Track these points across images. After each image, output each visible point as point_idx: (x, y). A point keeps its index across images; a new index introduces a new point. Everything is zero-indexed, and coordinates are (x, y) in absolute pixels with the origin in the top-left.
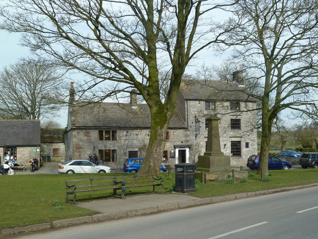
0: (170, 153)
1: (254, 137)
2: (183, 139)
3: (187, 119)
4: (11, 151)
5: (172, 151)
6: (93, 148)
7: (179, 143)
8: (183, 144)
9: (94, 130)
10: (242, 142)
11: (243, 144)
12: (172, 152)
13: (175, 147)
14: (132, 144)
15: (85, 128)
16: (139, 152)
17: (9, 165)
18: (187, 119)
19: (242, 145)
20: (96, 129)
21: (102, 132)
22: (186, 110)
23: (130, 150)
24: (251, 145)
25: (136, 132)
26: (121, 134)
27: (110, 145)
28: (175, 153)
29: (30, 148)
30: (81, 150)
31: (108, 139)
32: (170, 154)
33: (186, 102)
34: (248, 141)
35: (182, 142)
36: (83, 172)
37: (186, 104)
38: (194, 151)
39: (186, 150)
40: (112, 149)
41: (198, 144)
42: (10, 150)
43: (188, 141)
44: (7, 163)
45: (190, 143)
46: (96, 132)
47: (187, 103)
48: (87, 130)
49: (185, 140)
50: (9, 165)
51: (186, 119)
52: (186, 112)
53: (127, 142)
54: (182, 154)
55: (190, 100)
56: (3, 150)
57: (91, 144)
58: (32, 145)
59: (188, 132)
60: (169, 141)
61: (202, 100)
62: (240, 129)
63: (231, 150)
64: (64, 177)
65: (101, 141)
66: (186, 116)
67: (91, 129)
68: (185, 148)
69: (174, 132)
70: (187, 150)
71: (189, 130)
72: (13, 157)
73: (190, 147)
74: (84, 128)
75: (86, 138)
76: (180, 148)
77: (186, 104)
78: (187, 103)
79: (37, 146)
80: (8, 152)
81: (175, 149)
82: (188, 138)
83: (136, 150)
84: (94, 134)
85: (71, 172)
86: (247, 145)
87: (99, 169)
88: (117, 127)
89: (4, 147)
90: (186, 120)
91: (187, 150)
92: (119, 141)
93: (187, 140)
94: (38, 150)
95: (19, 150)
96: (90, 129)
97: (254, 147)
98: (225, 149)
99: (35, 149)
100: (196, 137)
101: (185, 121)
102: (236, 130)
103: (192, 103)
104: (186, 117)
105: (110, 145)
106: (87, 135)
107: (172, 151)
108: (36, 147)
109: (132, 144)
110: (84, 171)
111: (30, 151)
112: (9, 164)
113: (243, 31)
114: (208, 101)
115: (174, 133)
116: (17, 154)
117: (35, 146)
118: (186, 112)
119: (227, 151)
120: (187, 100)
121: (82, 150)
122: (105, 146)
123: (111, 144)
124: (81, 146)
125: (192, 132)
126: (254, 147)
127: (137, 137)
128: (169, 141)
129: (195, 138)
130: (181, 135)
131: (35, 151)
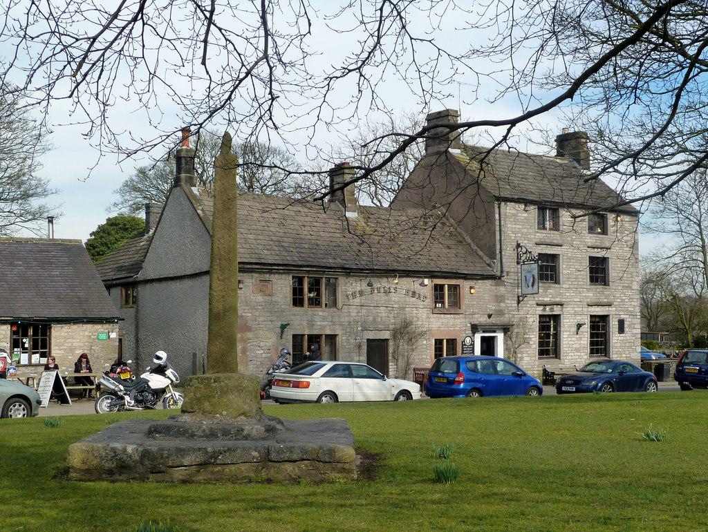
0: (463, 345)
1: (634, 306)
2: (492, 307)
3: (501, 252)
4: (33, 335)
5: (468, 340)
6: (279, 330)
7: (483, 319)
8: (493, 320)
9: (282, 273)
10: (611, 317)
11: (614, 324)
12: (468, 342)
13: (475, 328)
14: (374, 320)
15: (257, 267)
16: (391, 343)
17: (168, 378)
18: (501, 252)
19: (611, 327)
20: (287, 272)
21: (300, 281)
22: (498, 228)
23: (372, 335)
24: (629, 326)
25: (384, 283)
26: (348, 287)
27: (317, 320)
28: (473, 345)
29: (89, 326)
30: (249, 335)
31: (315, 302)
32: (463, 348)
33: (496, 206)
34: (623, 317)
35: (490, 316)
36: (360, 398)
37: (497, 210)
38: (514, 339)
39: (493, 337)
40: (328, 332)
41: (523, 320)
42: (31, 332)
43: (500, 313)
44: (160, 370)
45: (505, 319)
46: (287, 282)
47: (499, 207)
48: (264, 273)
49: (495, 310)
50: (168, 378)
51: (498, 252)
52: (498, 233)
53: (364, 311)
54: (488, 345)
55: (507, 200)
56: (9, 332)
57: (274, 319)
58: (97, 319)
59: (502, 289)
60: (460, 311)
61: (532, 202)
62: (557, 281)
63: (589, 339)
64: (485, 410)
65: (298, 309)
66: (498, 243)
67: (275, 273)
68: (495, 332)
69: (471, 288)
70: (500, 337)
71: (503, 284)
72: (38, 355)
73: (506, 329)
74: (254, 266)
75: (260, 298)
76: (484, 332)
77: (497, 210)
78: (499, 207)
79: (113, 322)
80: (24, 340)
81: (474, 336)
82: (502, 304)
83: (386, 335)
84: (283, 286)
85: (401, 397)
86: (621, 329)
87: (397, 388)
88: (339, 268)
89: (12, 324)
90: (498, 256)
91: (500, 337)
92: (345, 309)
93: (500, 311)
94: (113, 335)
95: (58, 333)
96: (270, 272)
97: (634, 331)
98: (578, 336)
99: (103, 333)
100: (519, 302)
101: (493, 256)
102: (600, 288)
103: (509, 209)
104: (498, 247)
105: (317, 320)
106: (264, 287)
107: (468, 340)
108: (107, 326)
109: (374, 320)
110: (365, 395)
111: (90, 336)
112: (169, 372)
113: (47, 19)
114: (542, 207)
115: (472, 291)
116: (53, 348)
117: (109, 321)
118: (498, 233)
119: (582, 342)
120: (500, 199)
121: (251, 336)
122: (311, 324)
123: (324, 319)
124: (250, 324)
125: (510, 288)
126: (634, 331)
127: (386, 298)
128: (460, 311)
129: (516, 305)
130: (487, 297)
131: (103, 336)
